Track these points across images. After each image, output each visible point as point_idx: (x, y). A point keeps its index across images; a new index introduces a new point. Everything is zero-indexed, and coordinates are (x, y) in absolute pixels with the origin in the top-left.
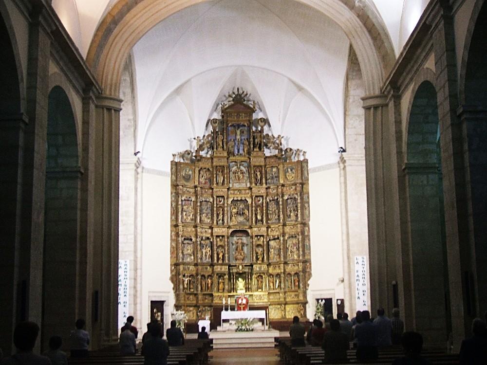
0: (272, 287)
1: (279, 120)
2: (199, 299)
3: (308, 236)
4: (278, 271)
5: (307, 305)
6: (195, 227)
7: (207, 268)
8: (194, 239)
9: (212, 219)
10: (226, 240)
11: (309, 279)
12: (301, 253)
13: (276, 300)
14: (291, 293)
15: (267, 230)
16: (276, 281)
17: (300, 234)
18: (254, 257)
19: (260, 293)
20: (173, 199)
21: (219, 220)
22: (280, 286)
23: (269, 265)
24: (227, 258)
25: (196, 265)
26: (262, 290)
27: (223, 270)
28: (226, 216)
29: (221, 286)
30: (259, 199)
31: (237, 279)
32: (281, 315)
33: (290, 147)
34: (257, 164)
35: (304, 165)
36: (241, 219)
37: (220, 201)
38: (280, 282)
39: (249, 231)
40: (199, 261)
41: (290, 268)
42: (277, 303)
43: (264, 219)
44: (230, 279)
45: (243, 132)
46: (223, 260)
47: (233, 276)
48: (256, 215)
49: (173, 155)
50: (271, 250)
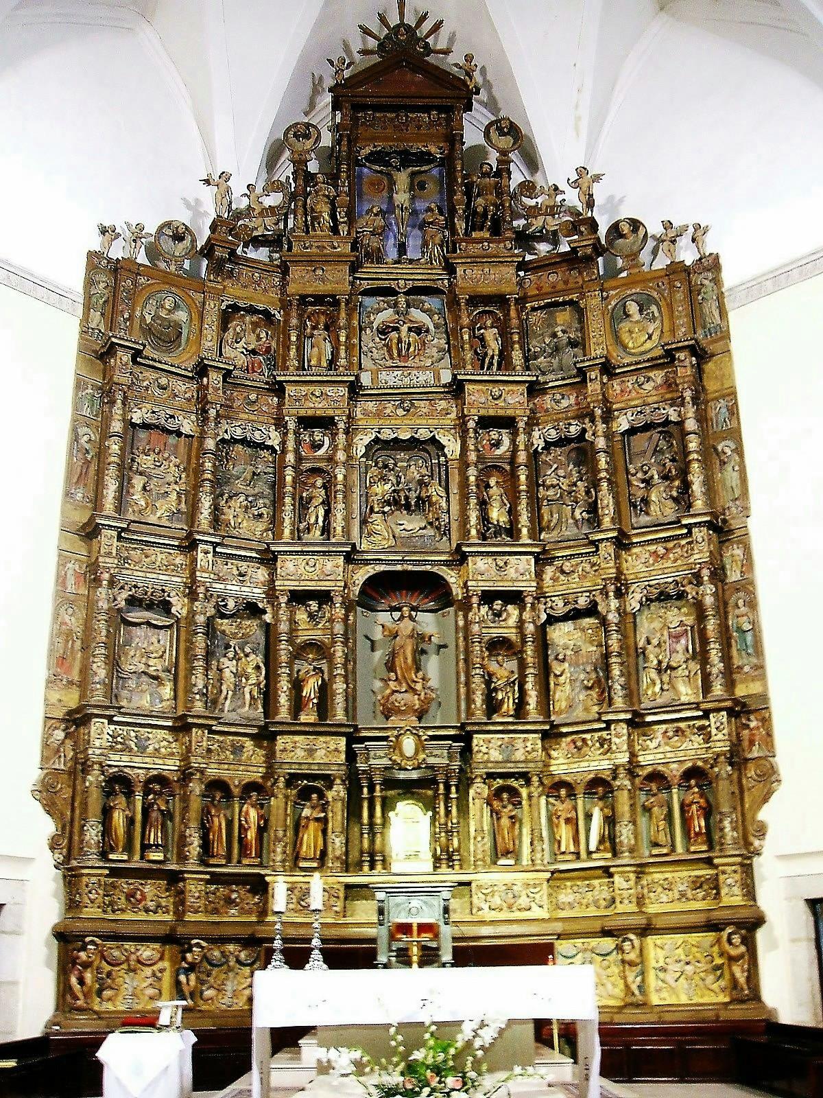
0: (567, 844)
2: (190, 900)
3: (747, 586)
4: (596, 763)
5: (760, 935)
6: (189, 545)
7: (237, 750)
8: (179, 606)
9: (275, 523)
10: (339, 612)
11: (765, 800)
12: (716, 665)
13: (592, 911)
14: (669, 874)
15: (539, 575)
16: (589, 817)
17: (705, 573)
18: (479, 699)
19: (509, 877)
20: (86, 411)
21: (308, 530)
22: (610, 841)
23: (551, 735)
24: (339, 700)
25: (181, 727)
28: (341, 506)
29: (310, 839)
30: (494, 434)
31: (388, 805)
32: (619, 991)
33: (625, 213)
34: (487, 289)
35: (704, 279)
36: (412, 523)
37: (316, 446)
38: (611, 821)
40: (199, 707)
41: (659, 751)
42: (597, 926)
43: (524, 519)
44: (353, 811)
45: (422, 186)
46: (324, 707)
47: (372, 789)
49: (104, 231)
50: (557, 668)
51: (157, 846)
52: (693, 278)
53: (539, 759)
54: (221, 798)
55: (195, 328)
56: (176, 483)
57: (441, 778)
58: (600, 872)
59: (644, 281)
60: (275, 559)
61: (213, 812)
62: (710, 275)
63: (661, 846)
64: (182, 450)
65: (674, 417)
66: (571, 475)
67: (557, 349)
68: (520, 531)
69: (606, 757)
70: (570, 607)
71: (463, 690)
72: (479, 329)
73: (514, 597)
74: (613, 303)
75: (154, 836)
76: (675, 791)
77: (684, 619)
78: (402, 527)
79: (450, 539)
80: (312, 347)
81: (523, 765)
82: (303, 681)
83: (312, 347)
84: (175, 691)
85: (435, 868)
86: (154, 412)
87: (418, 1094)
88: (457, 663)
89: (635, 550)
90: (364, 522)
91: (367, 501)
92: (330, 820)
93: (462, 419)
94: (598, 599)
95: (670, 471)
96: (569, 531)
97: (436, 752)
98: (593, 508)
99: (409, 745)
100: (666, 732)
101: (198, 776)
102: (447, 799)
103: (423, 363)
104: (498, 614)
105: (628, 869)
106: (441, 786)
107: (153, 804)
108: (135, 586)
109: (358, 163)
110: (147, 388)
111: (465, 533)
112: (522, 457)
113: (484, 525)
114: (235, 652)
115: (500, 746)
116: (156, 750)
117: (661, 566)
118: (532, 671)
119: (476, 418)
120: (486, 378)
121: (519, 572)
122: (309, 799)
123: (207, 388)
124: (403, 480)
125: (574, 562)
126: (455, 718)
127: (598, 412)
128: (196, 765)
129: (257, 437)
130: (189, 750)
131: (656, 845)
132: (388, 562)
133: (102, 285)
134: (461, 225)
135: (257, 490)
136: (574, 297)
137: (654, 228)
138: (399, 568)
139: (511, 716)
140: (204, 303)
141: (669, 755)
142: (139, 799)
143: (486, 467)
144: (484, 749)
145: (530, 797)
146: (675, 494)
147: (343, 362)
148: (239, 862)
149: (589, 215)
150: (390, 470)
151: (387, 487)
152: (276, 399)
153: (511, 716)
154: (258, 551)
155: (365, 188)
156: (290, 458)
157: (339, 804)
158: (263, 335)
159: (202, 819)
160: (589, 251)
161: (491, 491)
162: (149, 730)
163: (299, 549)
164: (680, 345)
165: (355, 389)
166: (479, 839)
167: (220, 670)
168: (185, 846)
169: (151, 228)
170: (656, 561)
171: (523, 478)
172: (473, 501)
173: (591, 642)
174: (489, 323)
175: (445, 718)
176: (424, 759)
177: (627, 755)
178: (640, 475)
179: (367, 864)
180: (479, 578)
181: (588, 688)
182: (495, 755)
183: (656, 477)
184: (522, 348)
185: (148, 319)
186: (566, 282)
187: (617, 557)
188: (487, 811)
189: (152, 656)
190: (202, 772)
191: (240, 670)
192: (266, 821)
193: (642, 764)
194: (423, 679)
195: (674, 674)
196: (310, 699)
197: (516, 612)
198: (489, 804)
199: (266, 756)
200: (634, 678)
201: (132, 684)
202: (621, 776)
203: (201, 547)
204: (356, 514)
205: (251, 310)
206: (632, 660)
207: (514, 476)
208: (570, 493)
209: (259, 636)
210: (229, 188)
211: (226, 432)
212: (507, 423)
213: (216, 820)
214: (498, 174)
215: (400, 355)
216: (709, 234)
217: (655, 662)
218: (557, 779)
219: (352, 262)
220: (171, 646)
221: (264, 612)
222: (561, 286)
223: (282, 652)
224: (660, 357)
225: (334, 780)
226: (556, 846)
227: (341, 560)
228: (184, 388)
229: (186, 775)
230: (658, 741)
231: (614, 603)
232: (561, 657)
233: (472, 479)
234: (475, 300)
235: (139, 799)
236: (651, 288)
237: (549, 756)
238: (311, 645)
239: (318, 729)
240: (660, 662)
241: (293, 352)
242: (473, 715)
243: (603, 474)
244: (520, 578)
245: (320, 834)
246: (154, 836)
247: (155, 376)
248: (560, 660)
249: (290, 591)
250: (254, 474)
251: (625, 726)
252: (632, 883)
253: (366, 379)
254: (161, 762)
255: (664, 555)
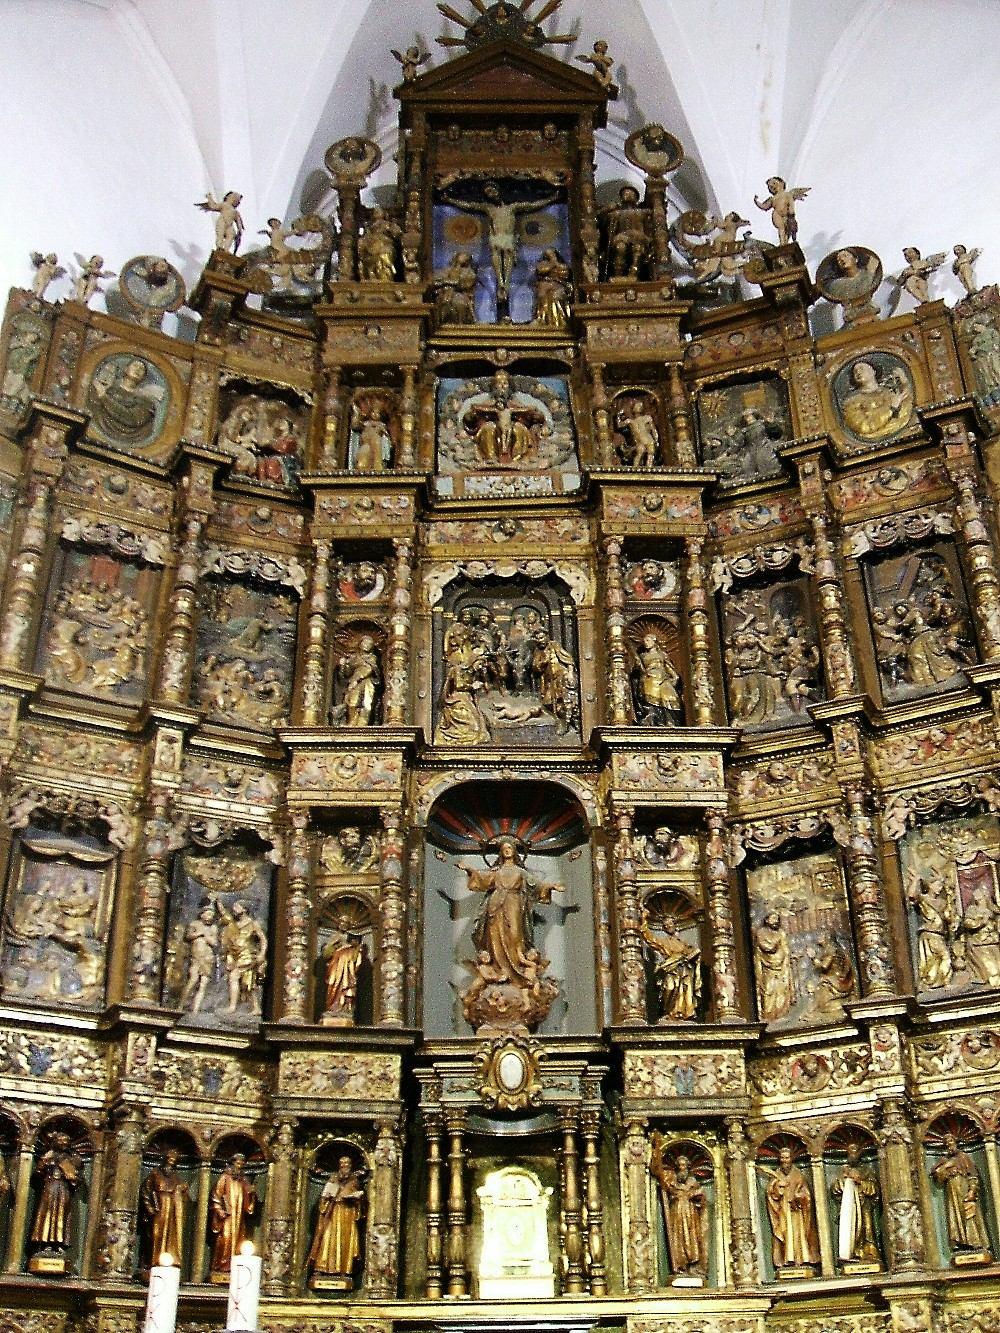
0: (796, 1246)
1: (764, 139)
4: (848, 1100)
6: (143, 731)
7: (211, 1077)
8: (122, 830)
9: (292, 705)
10: (393, 841)
15: (732, 785)
16: (835, 1197)
18: (634, 991)
22: (877, 1240)
23: (761, 1052)
24: (392, 991)
25: (110, 1032)
26: (708, 1275)
27: (355, 1087)
29: (335, 1239)
30: (651, 568)
36: (518, 708)
37: (363, 587)
38: (875, 1205)
39: (584, 791)
40: (144, 996)
43: (704, 692)
45: (533, 229)
47: (445, 1148)
48: (636, 676)
49: (38, 261)
50: (766, 939)
51: (55, 1245)
52: (959, 325)
53: (741, 1092)
54: (178, 1161)
55: (177, 410)
56: (130, 635)
57: (569, 1128)
58: (860, 1299)
59: (878, 335)
60: (288, 760)
61: (162, 1186)
62: (987, 318)
63: (971, 1248)
64: (144, 588)
65: (943, 527)
66: (777, 629)
67: (746, 442)
68: (697, 713)
69: (859, 1088)
70: (786, 836)
71: (605, 977)
72: (624, 417)
73: (691, 821)
74: (833, 370)
75: (50, 1228)
76: (990, 1146)
77: (982, 847)
78: (502, 713)
79: (581, 732)
80: (361, 443)
81: (714, 1104)
82: (331, 958)
83: (361, 443)
84: (107, 972)
85: (560, 1294)
86: (100, 526)
87: (216, 1311)
88: (596, 932)
89: (892, 739)
90: (439, 705)
91: (445, 674)
92: (372, 1204)
93: (600, 541)
94: (833, 821)
95: (943, 611)
96: (781, 714)
97: (558, 1081)
98: (819, 681)
99: (511, 1067)
100: (967, 1041)
101: (134, 1117)
102: (581, 1167)
103: (534, 466)
104: (663, 851)
105: (915, 1291)
106: (570, 1142)
107: (52, 1168)
108: (49, 794)
109: (438, 198)
110: (91, 490)
111: (605, 712)
112: (697, 598)
113: (637, 709)
114: (217, 911)
115: (673, 1071)
116: (64, 1071)
117: (938, 761)
118: (724, 941)
119: (621, 539)
120: (634, 478)
121: (697, 779)
122: (336, 1167)
123: (186, 490)
124: (503, 640)
125: (789, 762)
126: (593, 1025)
127: (819, 523)
128: (133, 1098)
129: (268, 573)
130: (121, 1072)
131: (964, 1247)
132: (477, 765)
133: (30, 337)
134: (591, 271)
135: (264, 655)
136: (772, 365)
137: (893, 264)
138: (496, 775)
139: (691, 1018)
140: (192, 376)
141: (974, 1082)
142: (26, 1160)
143: (637, 620)
144: (644, 1076)
145: (727, 1161)
146: (953, 645)
147: (407, 458)
148: (207, 1279)
149: (791, 241)
150: (484, 626)
151: (480, 651)
152: (300, 518)
153: (691, 1018)
154: (261, 747)
155: (447, 233)
156: (320, 601)
157: (388, 1173)
158: (284, 426)
159: (142, 1199)
160: (793, 291)
161: (647, 657)
162: (55, 1036)
163: (328, 739)
164: (949, 410)
165: (426, 501)
166: (638, 1237)
167: (189, 941)
168: (103, 1246)
169: (114, 264)
170: (929, 754)
171: (700, 630)
172: (619, 664)
173: (824, 896)
174: (639, 406)
175: (580, 1023)
176: (539, 1092)
177: (902, 1080)
178: (892, 622)
179: (435, 1283)
180: (631, 787)
181: (824, 971)
182: (664, 1086)
183: (920, 621)
184: (692, 437)
185: (101, 391)
186: (757, 345)
187: (864, 749)
188: (651, 1188)
189: (74, 912)
190: (143, 1109)
191: (223, 948)
192: (259, 1206)
193: (927, 1098)
194: (538, 961)
195: (972, 941)
196: (340, 990)
197: (695, 847)
198: (655, 1175)
199: (264, 1090)
200: (902, 949)
201: (30, 956)
202: (893, 1118)
203: (164, 731)
204: (426, 693)
205: (268, 392)
206: (897, 919)
207: (685, 630)
208: (779, 656)
209: (260, 888)
210: (237, 218)
211: (217, 562)
212: (671, 549)
213: (167, 1201)
214: (648, 203)
215: (499, 457)
216: (978, 262)
217: (939, 921)
218: (773, 1131)
219: (425, 319)
220: (106, 898)
221: (269, 846)
222: (750, 350)
223: (295, 910)
224: (916, 438)
225: (380, 1130)
226: (777, 1251)
227: (398, 759)
228: (151, 494)
229: (115, 1113)
230: (951, 1057)
231: (863, 822)
232: (772, 920)
233: (617, 631)
234: (616, 373)
235: (26, 1160)
236: (893, 343)
237: (759, 1090)
238: (347, 901)
239: (352, 1039)
240: (946, 923)
241: (328, 448)
242: (624, 1017)
243: (833, 617)
244: (700, 786)
245: (353, 1228)
246: (50, 1228)
247: (105, 473)
248: (770, 926)
249: (312, 809)
250: (262, 630)
251: (893, 1029)
252: (925, 1318)
253: (444, 487)
254: (70, 1091)
255: (943, 742)
